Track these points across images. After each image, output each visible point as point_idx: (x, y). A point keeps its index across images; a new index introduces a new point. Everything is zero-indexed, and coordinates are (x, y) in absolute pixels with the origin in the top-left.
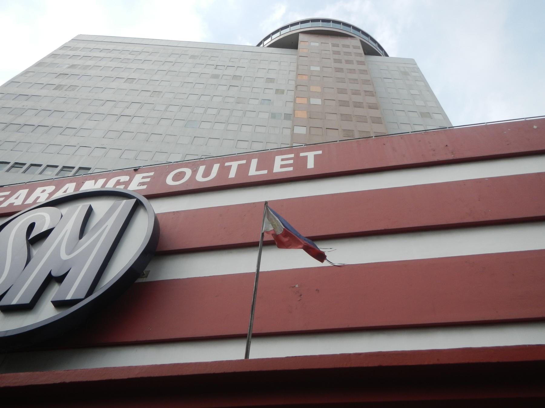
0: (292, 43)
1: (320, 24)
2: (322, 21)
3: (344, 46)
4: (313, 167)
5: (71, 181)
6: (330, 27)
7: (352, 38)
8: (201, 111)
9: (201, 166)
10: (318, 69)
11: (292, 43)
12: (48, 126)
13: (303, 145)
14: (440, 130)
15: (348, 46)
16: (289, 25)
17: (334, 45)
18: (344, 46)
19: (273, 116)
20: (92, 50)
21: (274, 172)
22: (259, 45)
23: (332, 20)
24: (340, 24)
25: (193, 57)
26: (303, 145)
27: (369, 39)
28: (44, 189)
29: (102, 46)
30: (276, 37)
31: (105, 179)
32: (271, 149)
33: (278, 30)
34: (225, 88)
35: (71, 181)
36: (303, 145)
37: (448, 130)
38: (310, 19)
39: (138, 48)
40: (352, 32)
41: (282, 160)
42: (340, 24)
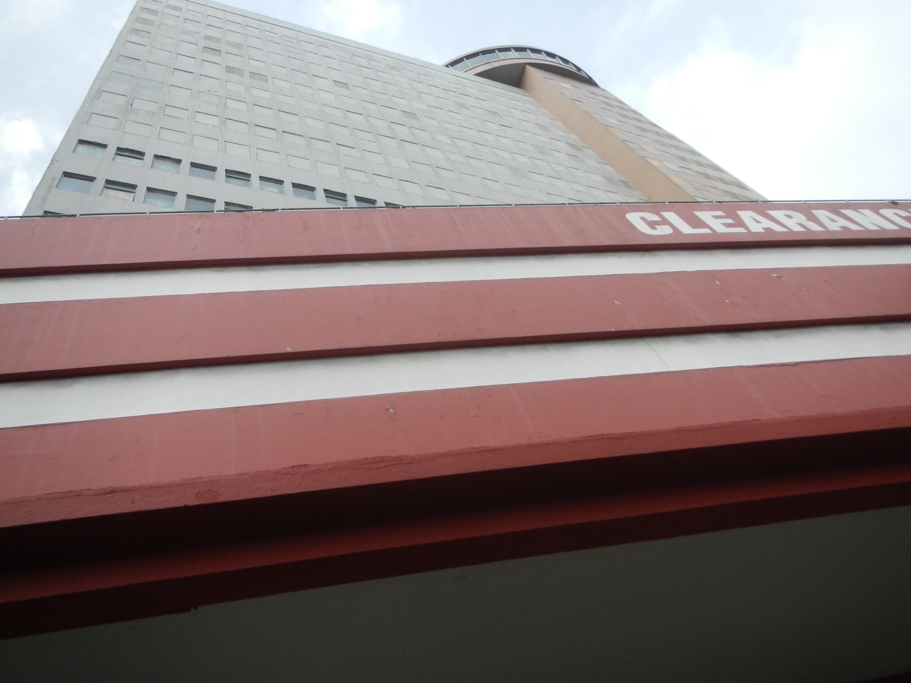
1: (513, 54)
11: (511, 77)
33: (475, 53)
37: (281, 212)
39: (292, 34)
40: (518, 57)
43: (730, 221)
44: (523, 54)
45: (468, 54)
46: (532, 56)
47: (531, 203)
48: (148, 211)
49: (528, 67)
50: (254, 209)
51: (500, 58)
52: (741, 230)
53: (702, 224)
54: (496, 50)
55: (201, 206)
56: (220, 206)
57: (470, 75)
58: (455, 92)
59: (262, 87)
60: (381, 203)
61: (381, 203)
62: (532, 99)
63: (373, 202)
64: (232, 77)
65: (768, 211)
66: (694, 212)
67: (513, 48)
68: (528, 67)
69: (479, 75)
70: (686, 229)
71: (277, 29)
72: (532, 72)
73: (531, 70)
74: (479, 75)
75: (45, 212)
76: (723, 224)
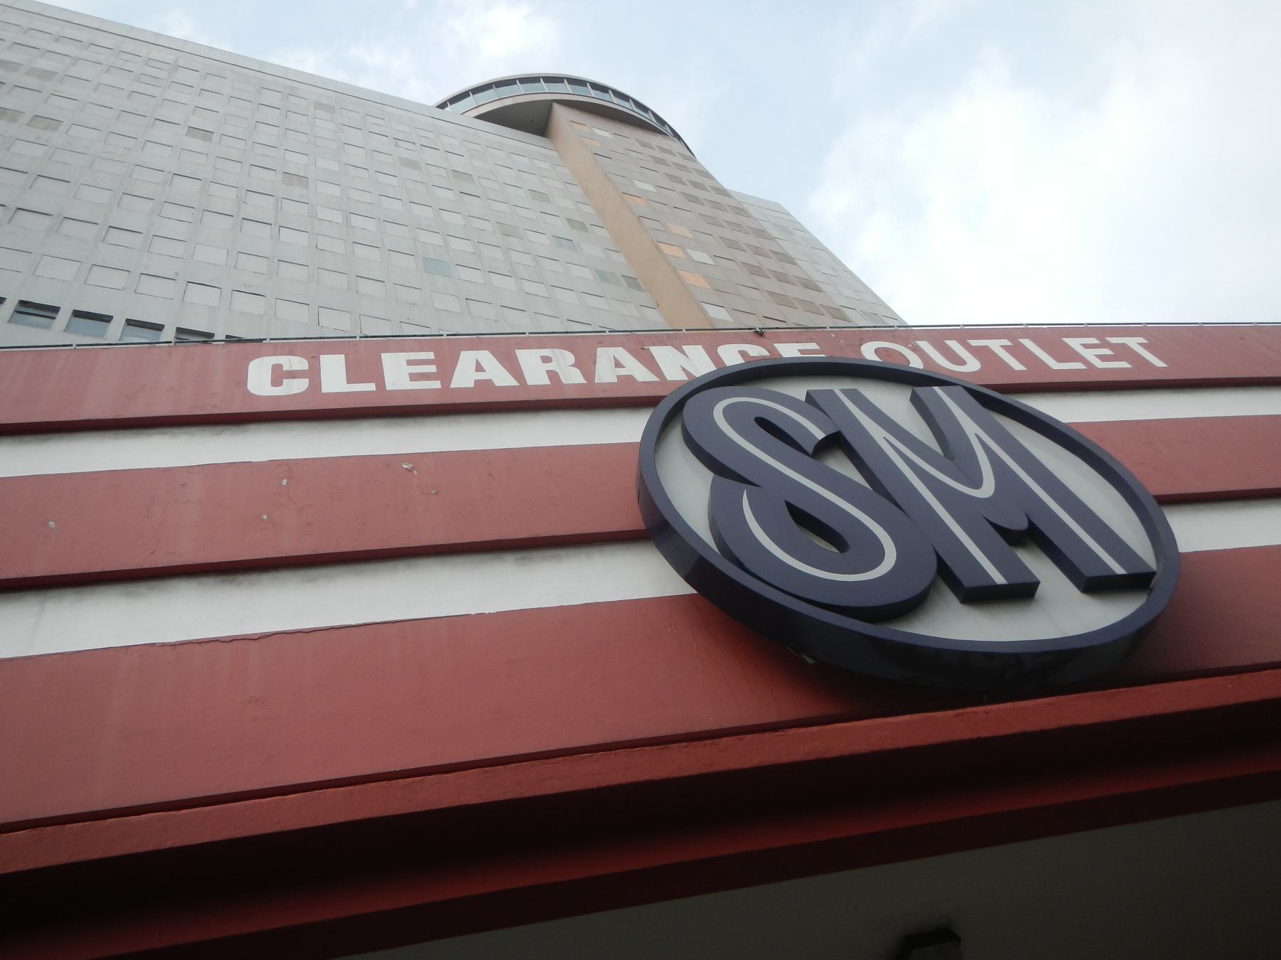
0: (533, 121)
1: (519, 88)
2: (473, 94)
3: (663, 150)
4: (473, 386)
5: (600, 343)
6: (617, 103)
7: (665, 136)
8: (338, 217)
9: (703, 346)
10: (649, 187)
11: (533, 121)
12: (51, 215)
13: (605, 332)
14: (672, 332)
15: (670, 153)
16: (446, 102)
17: (644, 145)
18: (663, 150)
19: (603, 276)
20: (58, 39)
21: (451, 386)
22: (442, 106)
23: (542, 77)
24: (539, 81)
25: (319, 106)
26: (605, 332)
27: (612, 95)
28: (1084, 349)
29: (55, 29)
30: (491, 101)
31: (1098, 342)
32: (271, 339)
33: (488, 84)
34: (450, 195)
35: (600, 343)
36: (607, 330)
37: (447, 339)
38: (446, 99)
39: (169, 57)
40: (571, 92)
41: (410, 363)
42: (539, 81)
43: (432, 369)
44: (580, 89)
45: (476, 86)
46: (592, 93)
47: (422, 334)
48: (74, 343)
49: (556, 106)
50: (215, 338)
51: (544, 89)
52: (371, 387)
53: (1074, 356)
54: (565, 81)
55: (147, 335)
56: (168, 334)
57: (469, 120)
58: (414, 143)
59: (38, 138)
60: (220, 336)
61: (220, 336)
62: (555, 154)
63: (211, 335)
64: (321, 113)
65: (1107, 338)
66: (1020, 340)
67: (566, 78)
68: (555, 105)
69: (480, 117)
70: (501, 378)
71: (129, 46)
72: (561, 114)
73: (559, 111)
74: (480, 117)
75: (227, 336)
76: (1096, 356)
